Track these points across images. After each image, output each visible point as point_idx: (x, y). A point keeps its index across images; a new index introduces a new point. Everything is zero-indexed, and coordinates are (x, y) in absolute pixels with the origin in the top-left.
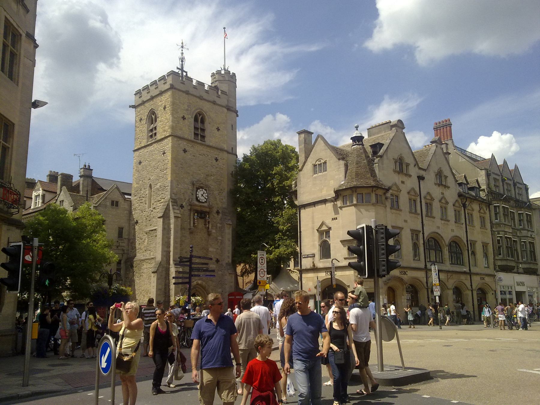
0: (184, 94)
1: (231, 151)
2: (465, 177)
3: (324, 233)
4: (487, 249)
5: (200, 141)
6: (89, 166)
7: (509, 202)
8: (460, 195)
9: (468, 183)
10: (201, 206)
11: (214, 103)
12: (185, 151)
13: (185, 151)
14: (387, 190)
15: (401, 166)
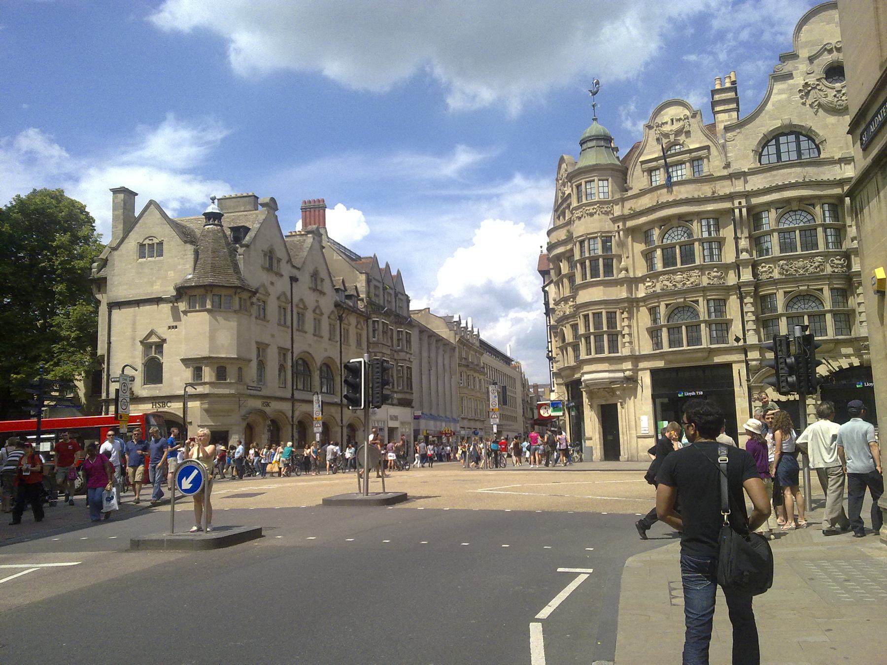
2: (343, 281)
3: (153, 348)
7: (390, 316)
8: (337, 305)
9: (346, 290)
14: (255, 293)
15: (271, 261)
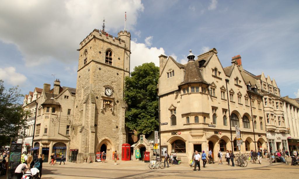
1: (126, 70)
2: (167, 142)
3: (173, 110)
11: (118, 46)
12: (100, 69)
13: (100, 69)
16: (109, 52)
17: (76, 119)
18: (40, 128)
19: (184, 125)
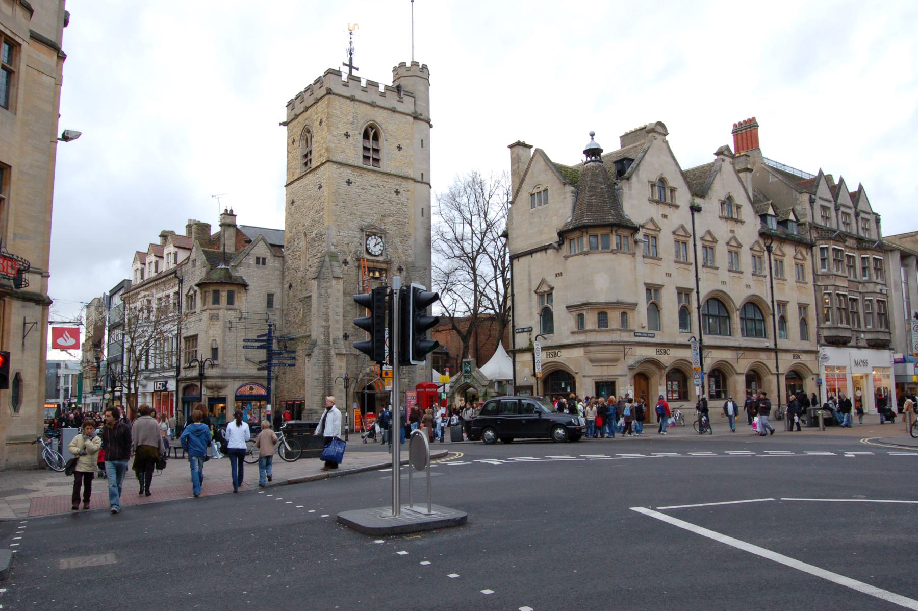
0: (348, 101)
1: (420, 179)
3: (546, 295)
4: (806, 313)
5: (371, 167)
6: (231, 211)
7: (844, 241)
10: (373, 261)
11: (394, 110)
12: (349, 183)
13: (349, 183)
16: (371, 133)
17: (291, 318)
18: (196, 346)
19: (573, 333)
